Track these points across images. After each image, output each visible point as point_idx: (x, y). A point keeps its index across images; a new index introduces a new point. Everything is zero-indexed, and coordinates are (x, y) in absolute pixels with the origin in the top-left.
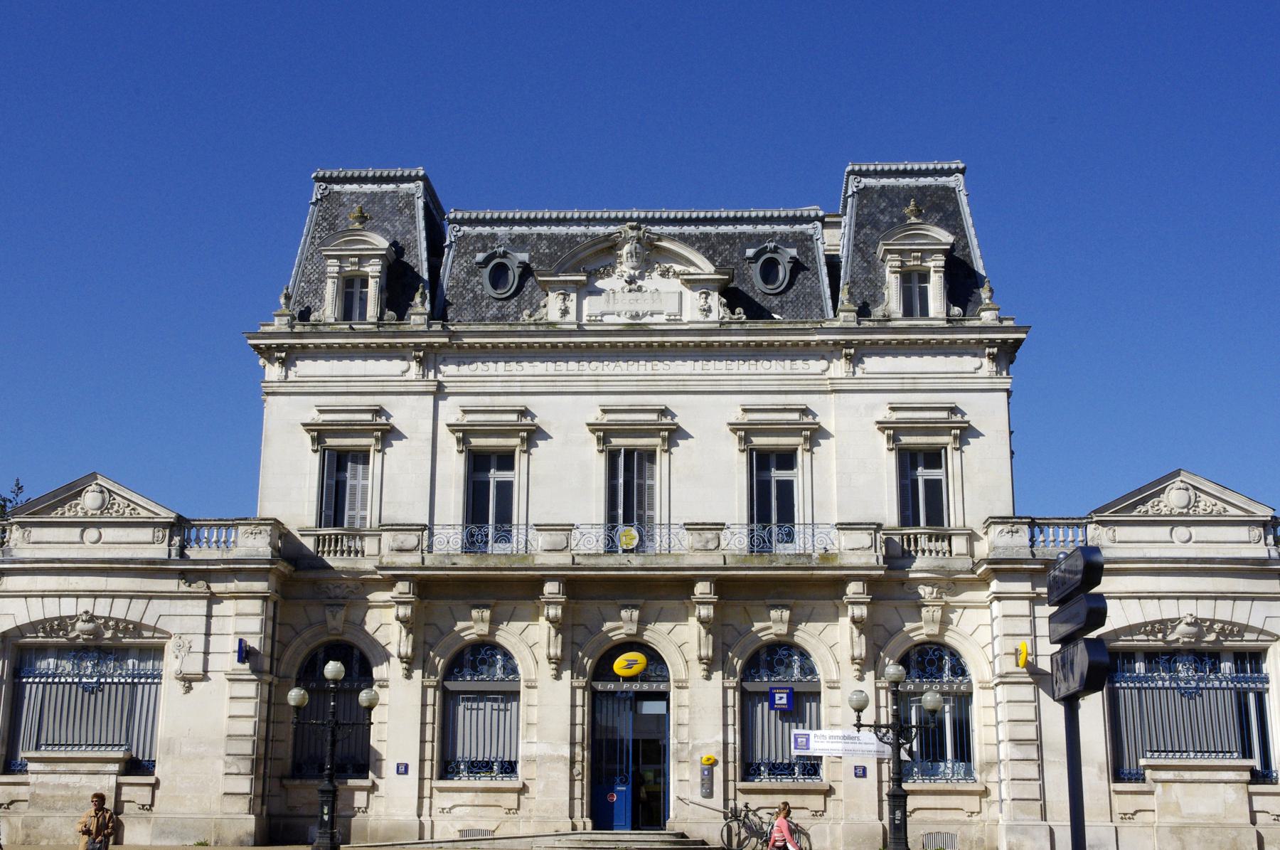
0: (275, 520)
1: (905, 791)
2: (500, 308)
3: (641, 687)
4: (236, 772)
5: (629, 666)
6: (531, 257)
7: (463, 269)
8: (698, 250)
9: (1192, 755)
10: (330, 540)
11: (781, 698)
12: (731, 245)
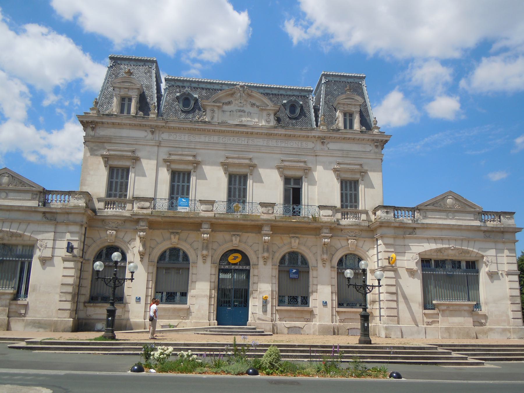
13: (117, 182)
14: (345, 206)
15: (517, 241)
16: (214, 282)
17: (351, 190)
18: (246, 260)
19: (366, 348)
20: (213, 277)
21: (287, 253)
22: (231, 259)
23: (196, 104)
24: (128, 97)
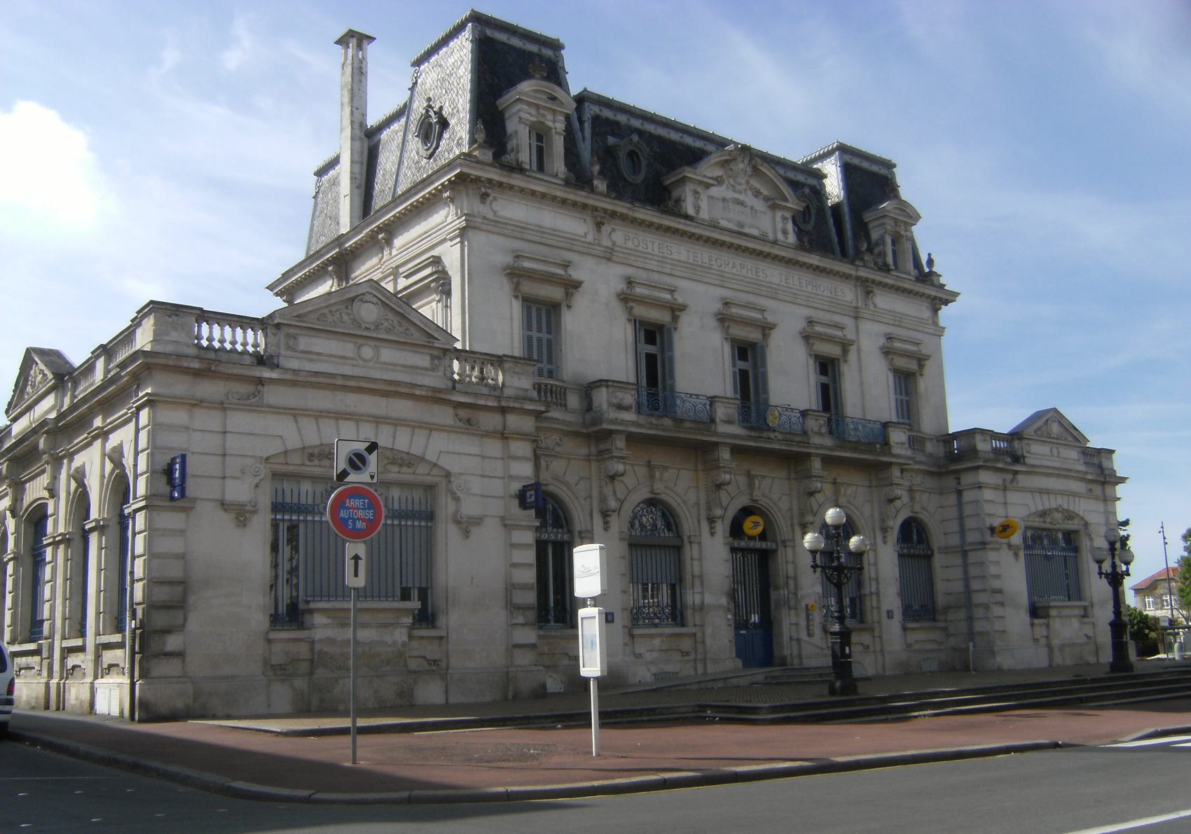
15: (1119, 499)
19: (845, 704)
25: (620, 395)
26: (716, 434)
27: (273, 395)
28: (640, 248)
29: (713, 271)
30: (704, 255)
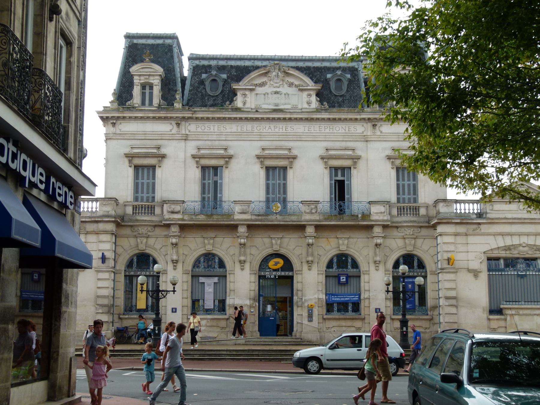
0: (115, 198)
1: (407, 319)
2: (214, 100)
3: (281, 273)
4: (102, 312)
5: (276, 264)
6: (228, 77)
7: (196, 82)
8: (305, 74)
9: (523, 303)
10: (142, 207)
11: (343, 279)
12: (320, 72)
13: (143, 183)
14: (401, 200)
16: (254, 290)
17: (279, 179)
18: (288, 265)
20: (253, 284)
21: (334, 256)
22: (271, 264)
23: (225, 87)
24: (148, 84)
25: (173, 206)
26: (234, 220)
27: (484, 228)
28: (206, 131)
29: (254, 134)
30: (248, 127)
